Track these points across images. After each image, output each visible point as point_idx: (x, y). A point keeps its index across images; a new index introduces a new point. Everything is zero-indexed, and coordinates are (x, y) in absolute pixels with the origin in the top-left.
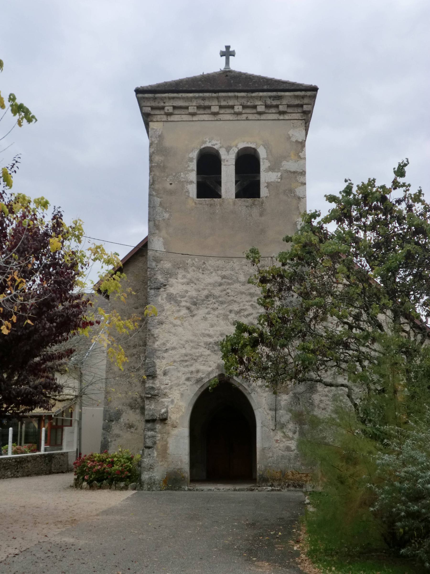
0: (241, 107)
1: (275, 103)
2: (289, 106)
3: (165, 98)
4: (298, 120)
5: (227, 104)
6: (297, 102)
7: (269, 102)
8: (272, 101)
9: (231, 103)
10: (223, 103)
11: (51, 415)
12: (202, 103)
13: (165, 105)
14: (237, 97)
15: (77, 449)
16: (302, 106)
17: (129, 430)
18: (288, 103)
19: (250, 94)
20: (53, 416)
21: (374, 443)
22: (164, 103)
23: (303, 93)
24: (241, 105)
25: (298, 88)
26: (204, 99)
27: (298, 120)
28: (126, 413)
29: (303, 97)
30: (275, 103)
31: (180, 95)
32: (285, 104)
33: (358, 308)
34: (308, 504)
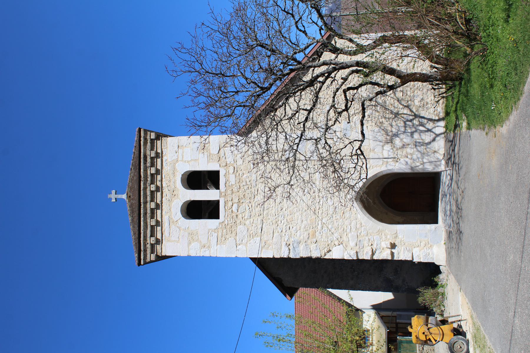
0: (151, 185)
1: (149, 160)
2: (152, 149)
3: (144, 243)
4: (161, 142)
5: (149, 196)
6: (149, 144)
7: (148, 164)
8: (148, 162)
9: (148, 193)
10: (149, 199)
11: (388, 332)
12: (148, 215)
13: (149, 243)
14: (145, 189)
15: (413, 312)
16: (151, 140)
17: (399, 272)
18: (149, 150)
19: (142, 179)
20: (388, 330)
21: (441, 110)
22: (148, 244)
23: (142, 139)
24: (150, 185)
25: (138, 143)
26: (145, 214)
27: (161, 142)
28: (386, 274)
29: (145, 139)
30: (149, 160)
31: (142, 232)
32: (150, 152)
33: (422, 153)
34: (325, 76)
